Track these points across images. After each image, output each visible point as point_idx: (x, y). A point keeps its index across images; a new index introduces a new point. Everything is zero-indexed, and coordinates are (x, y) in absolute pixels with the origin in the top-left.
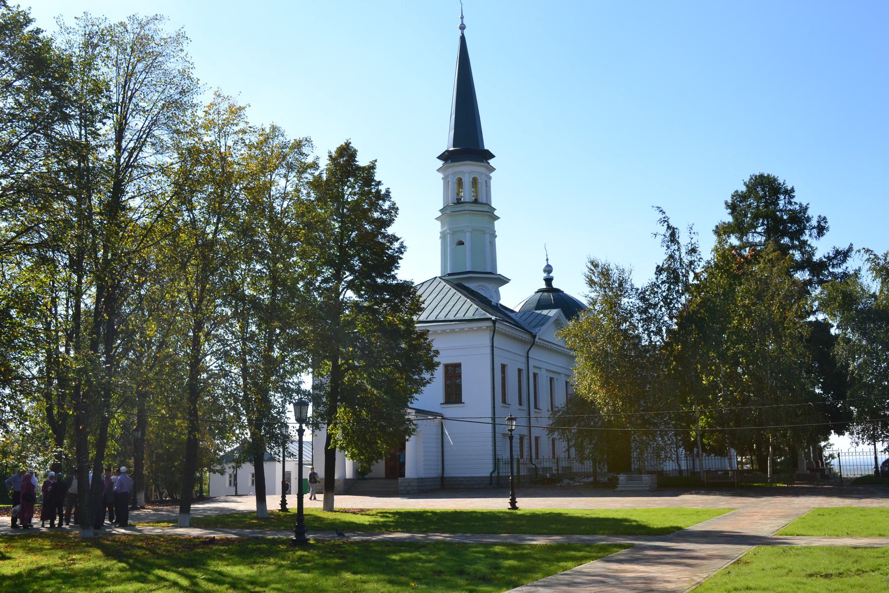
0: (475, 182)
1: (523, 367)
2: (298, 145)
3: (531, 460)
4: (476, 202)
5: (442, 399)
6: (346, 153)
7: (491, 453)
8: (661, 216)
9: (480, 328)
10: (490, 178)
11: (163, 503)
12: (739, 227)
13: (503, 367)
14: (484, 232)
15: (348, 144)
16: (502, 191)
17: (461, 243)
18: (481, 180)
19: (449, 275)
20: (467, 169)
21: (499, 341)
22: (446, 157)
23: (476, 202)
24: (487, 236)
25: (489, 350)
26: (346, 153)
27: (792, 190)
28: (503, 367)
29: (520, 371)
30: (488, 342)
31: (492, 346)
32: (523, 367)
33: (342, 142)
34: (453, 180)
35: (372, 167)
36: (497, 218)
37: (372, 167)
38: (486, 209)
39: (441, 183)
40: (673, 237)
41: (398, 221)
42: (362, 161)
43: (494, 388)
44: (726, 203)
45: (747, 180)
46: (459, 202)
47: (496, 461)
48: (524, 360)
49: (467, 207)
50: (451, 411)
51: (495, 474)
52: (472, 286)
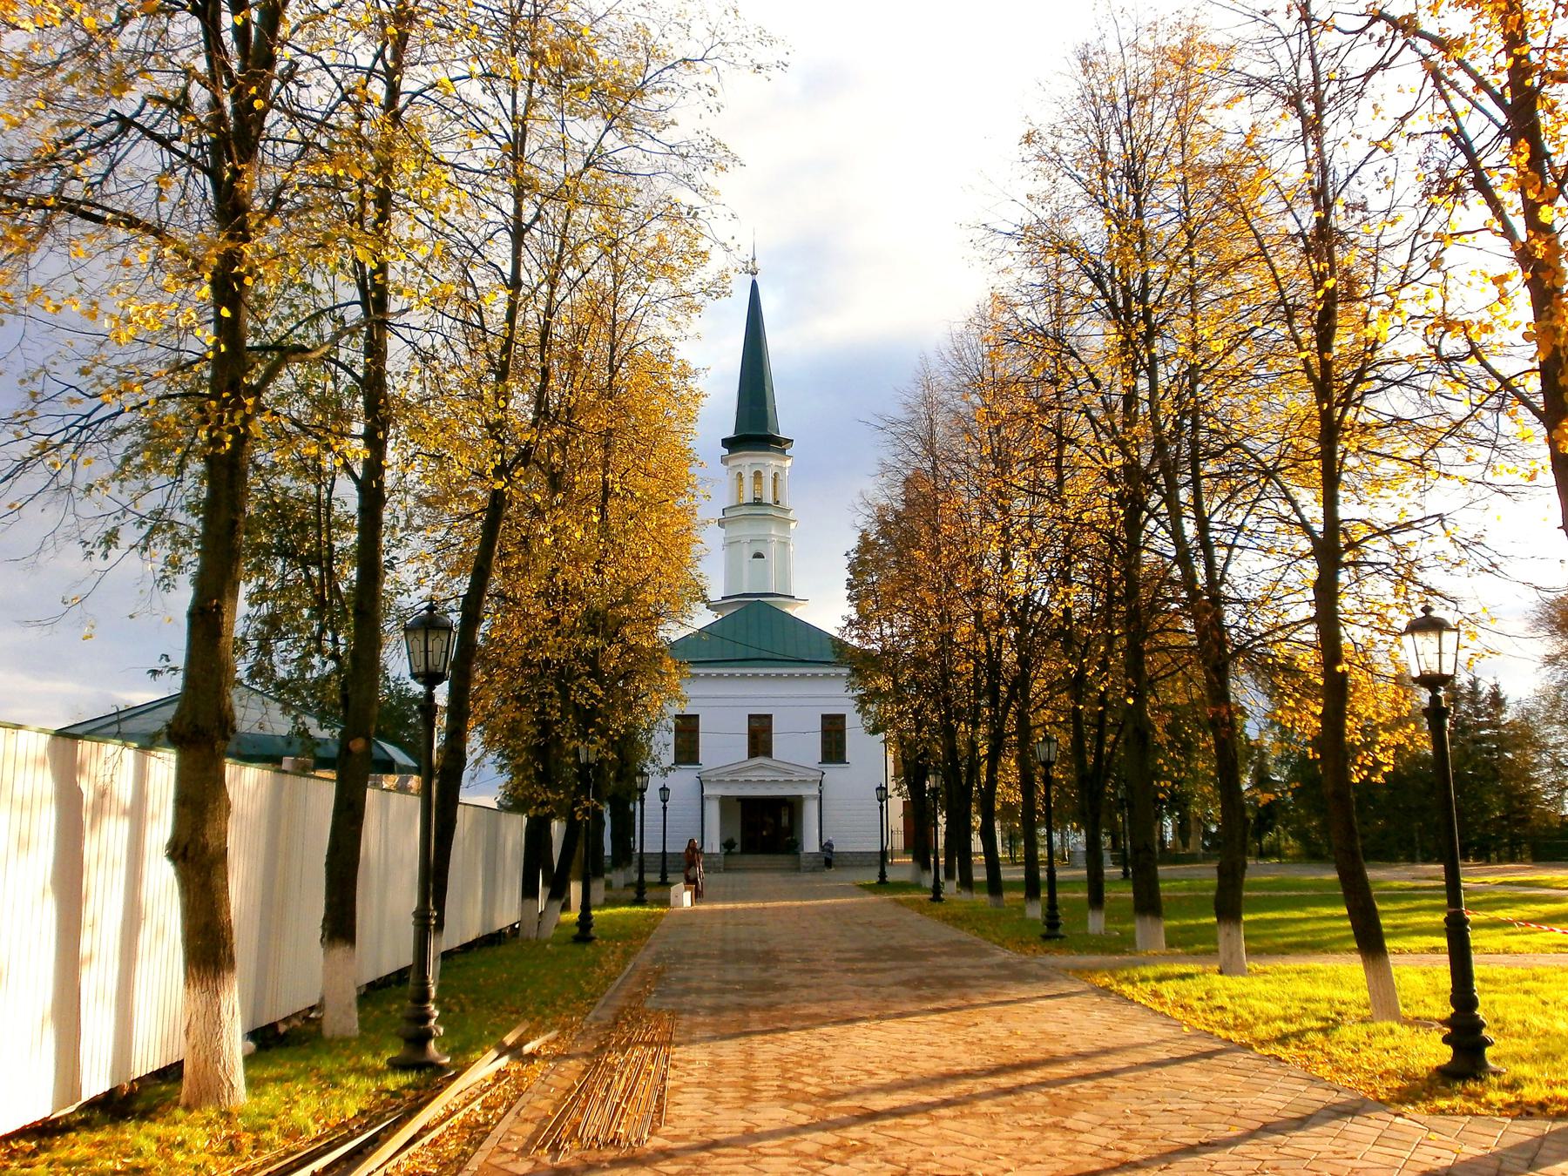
5: (818, 755)
17: (758, 556)
34: (748, 475)
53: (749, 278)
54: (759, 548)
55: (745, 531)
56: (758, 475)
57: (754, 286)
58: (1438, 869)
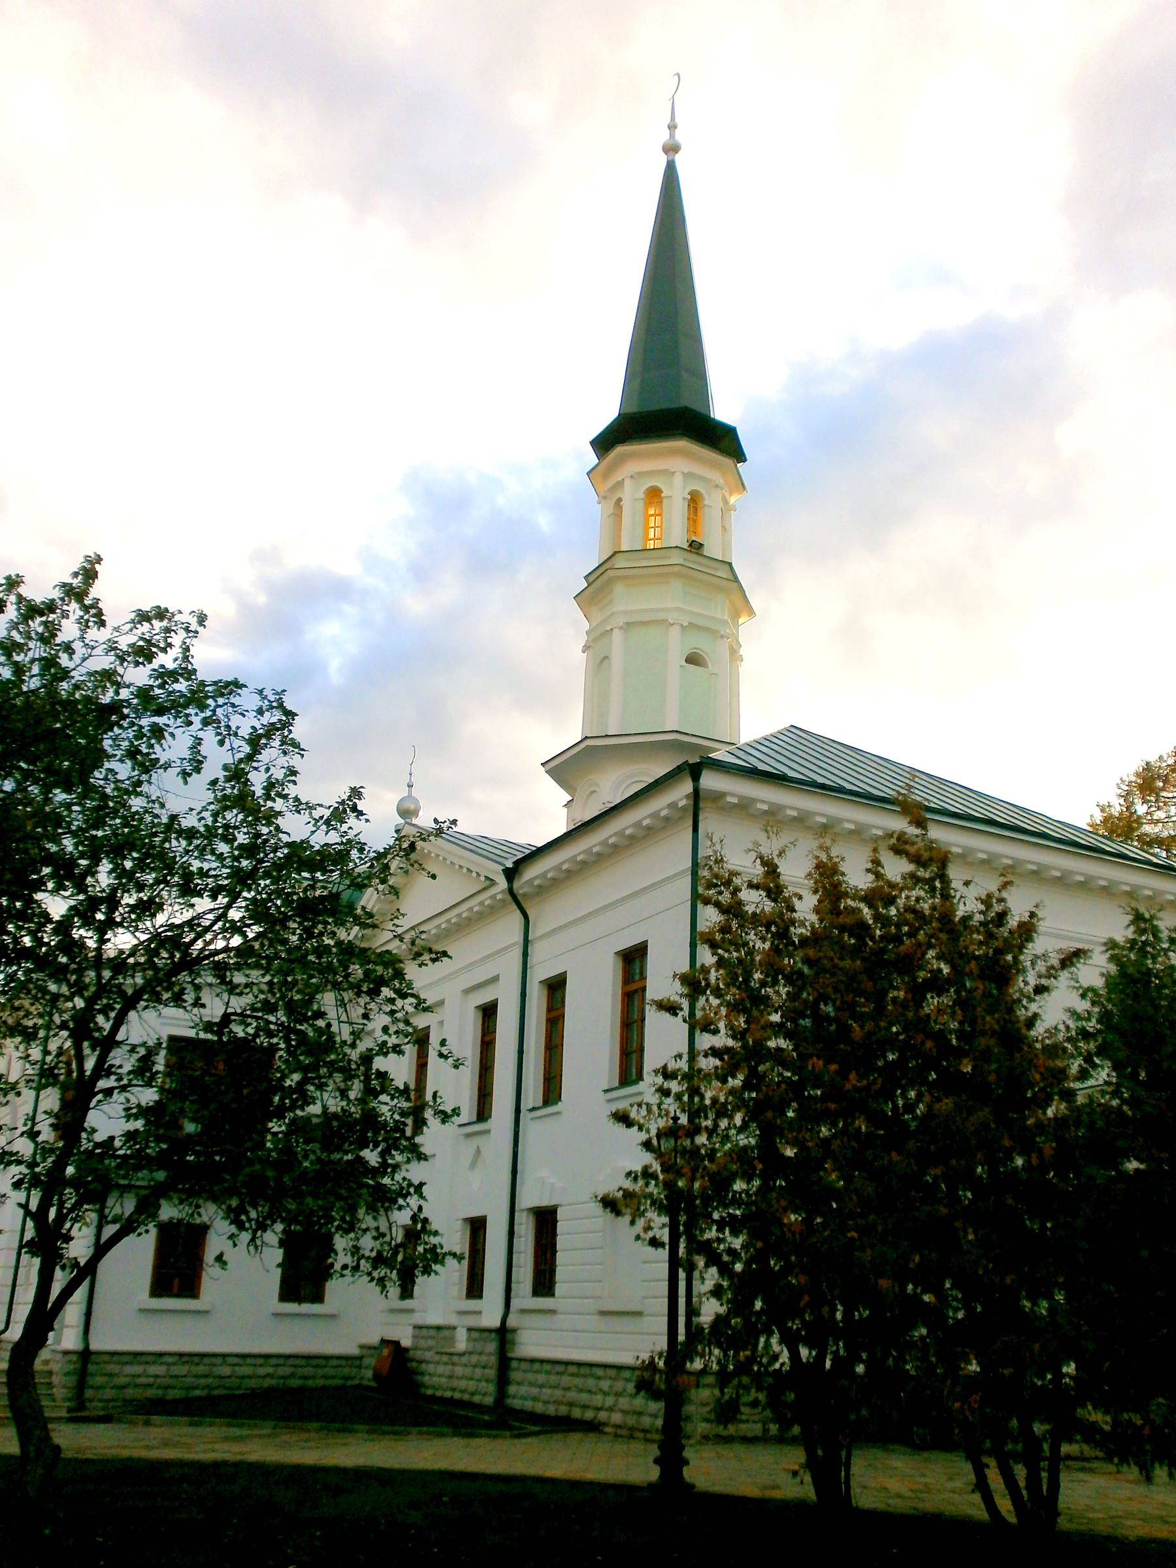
17: (693, 659)
22: (605, 443)
53: (663, 160)
54: (700, 643)
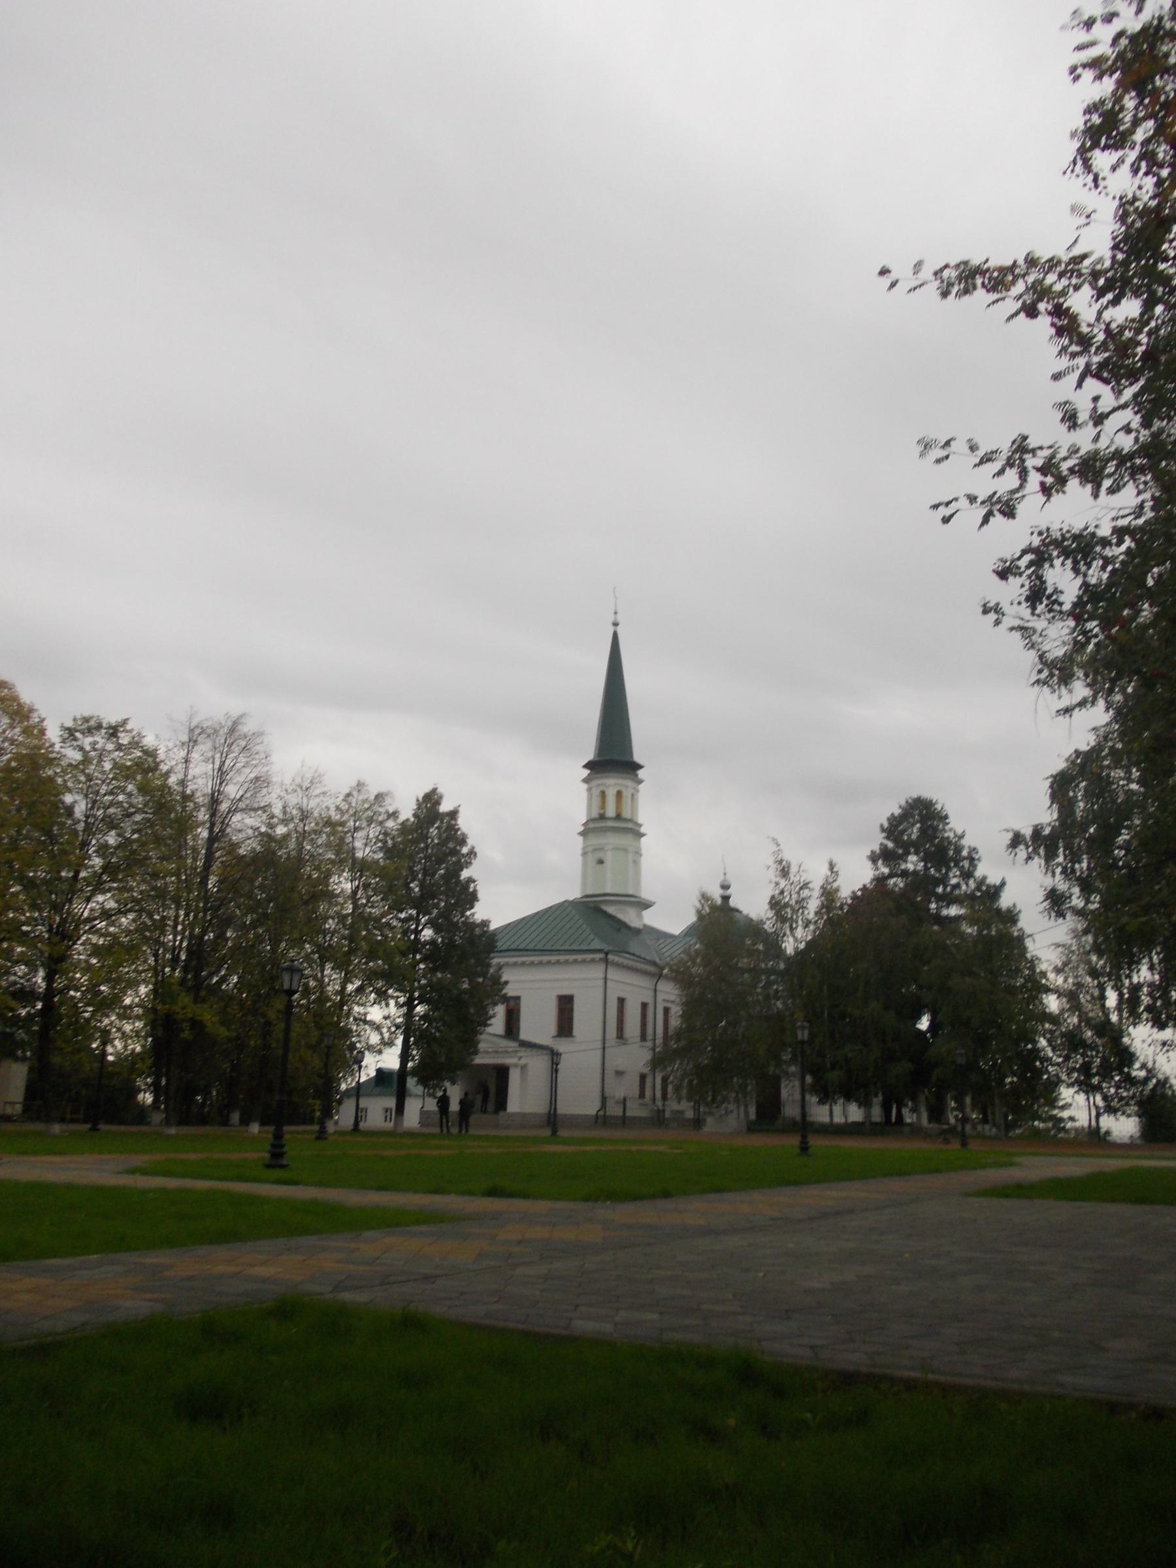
0: (619, 794)
1: (650, 1000)
2: (379, 797)
3: (654, 1099)
4: (618, 817)
6: (431, 800)
7: (598, 1089)
8: (775, 848)
9: (593, 960)
10: (638, 791)
11: (72, 1121)
12: (886, 855)
13: (621, 1001)
14: (626, 850)
15: (434, 791)
16: (649, 808)
17: (601, 862)
18: (627, 794)
19: (587, 896)
20: (612, 783)
21: (613, 974)
23: (618, 817)
24: (631, 857)
25: (601, 983)
26: (431, 800)
27: (946, 817)
28: (621, 1001)
29: (644, 1006)
30: (602, 975)
31: (606, 979)
32: (650, 1000)
33: (427, 789)
34: (596, 792)
35: (453, 814)
36: (643, 835)
37: (453, 814)
38: (630, 825)
39: (585, 795)
40: (785, 872)
41: (476, 863)
42: (445, 807)
43: (605, 1023)
44: (882, 826)
45: (903, 803)
46: (602, 817)
47: (604, 1099)
48: (651, 993)
49: (611, 824)
50: (562, 1046)
51: (601, 1113)
52: (611, 910)
54: (599, 855)
55: (595, 841)
56: (603, 794)
57: (615, 637)
58: (563, 1109)
